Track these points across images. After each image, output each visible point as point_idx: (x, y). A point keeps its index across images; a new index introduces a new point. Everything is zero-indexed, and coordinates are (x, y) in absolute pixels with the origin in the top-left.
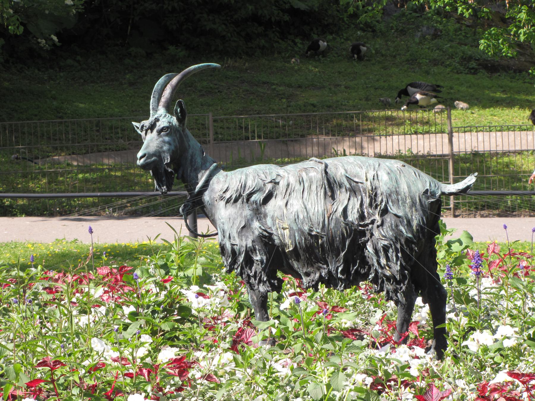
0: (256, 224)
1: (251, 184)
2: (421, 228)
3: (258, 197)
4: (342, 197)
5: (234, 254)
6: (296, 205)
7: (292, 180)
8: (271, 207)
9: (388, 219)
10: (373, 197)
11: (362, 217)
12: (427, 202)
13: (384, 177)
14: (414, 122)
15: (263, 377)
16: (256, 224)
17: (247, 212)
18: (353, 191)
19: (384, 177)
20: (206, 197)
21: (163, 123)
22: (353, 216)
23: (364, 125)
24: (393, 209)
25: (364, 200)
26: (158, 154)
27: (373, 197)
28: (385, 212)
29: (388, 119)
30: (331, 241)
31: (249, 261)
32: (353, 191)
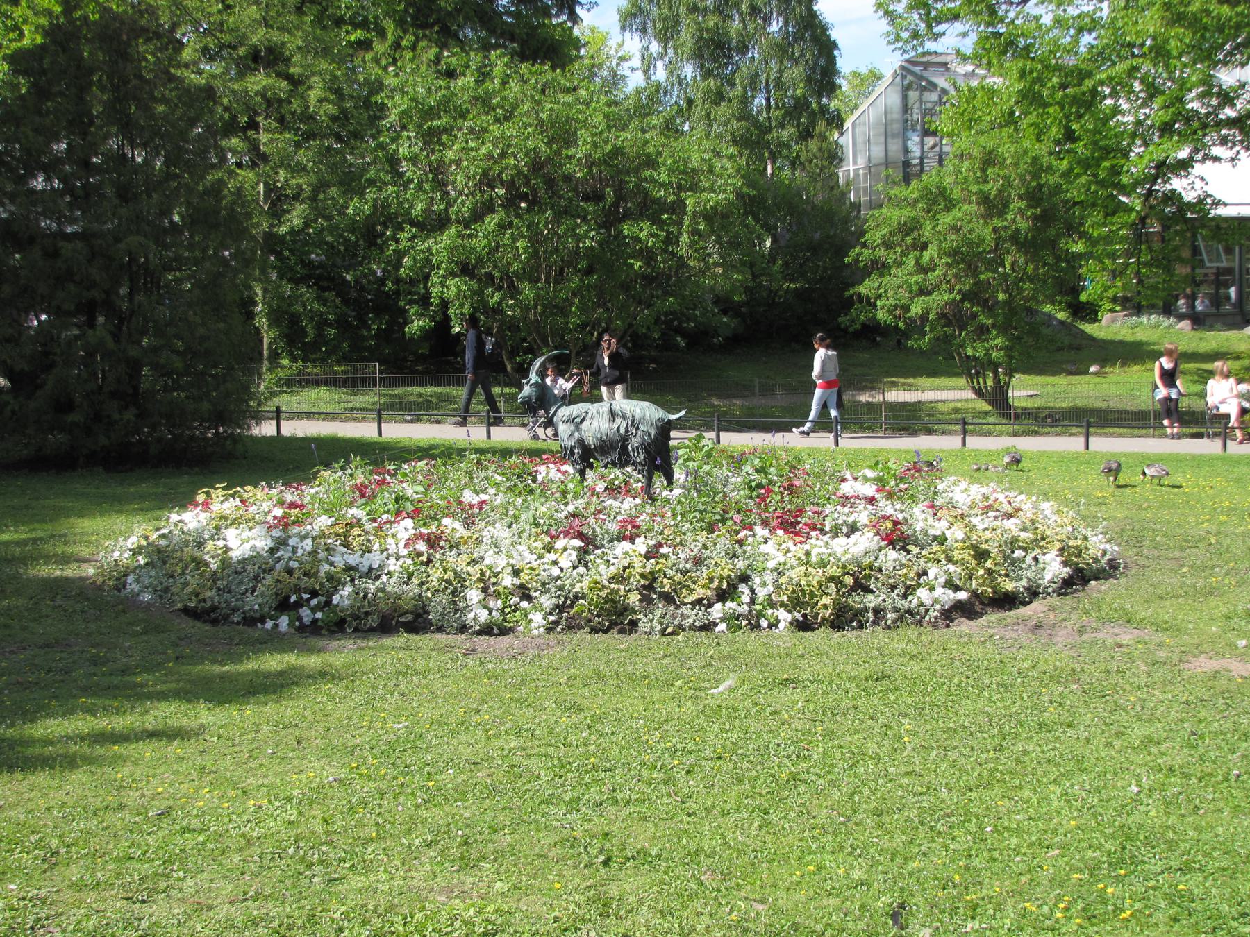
0: (576, 434)
1: (575, 414)
2: (656, 437)
3: (578, 420)
4: (618, 420)
5: (566, 449)
6: (595, 424)
7: (595, 411)
8: (586, 423)
9: (639, 433)
10: (633, 421)
11: (627, 431)
12: (660, 424)
13: (638, 411)
14: (904, 384)
15: (491, 552)
16: (576, 434)
17: (572, 427)
18: (624, 417)
19: (638, 411)
20: (555, 419)
21: (533, 381)
22: (622, 431)
23: (881, 386)
24: (642, 428)
25: (1134, 373)
26: (529, 397)
27: (633, 421)
28: (637, 429)
29: (893, 383)
30: (611, 444)
31: (572, 453)
32: (624, 417)
